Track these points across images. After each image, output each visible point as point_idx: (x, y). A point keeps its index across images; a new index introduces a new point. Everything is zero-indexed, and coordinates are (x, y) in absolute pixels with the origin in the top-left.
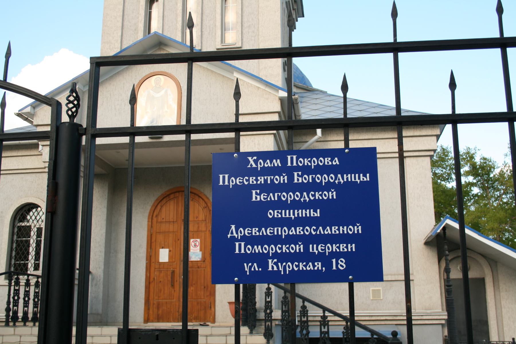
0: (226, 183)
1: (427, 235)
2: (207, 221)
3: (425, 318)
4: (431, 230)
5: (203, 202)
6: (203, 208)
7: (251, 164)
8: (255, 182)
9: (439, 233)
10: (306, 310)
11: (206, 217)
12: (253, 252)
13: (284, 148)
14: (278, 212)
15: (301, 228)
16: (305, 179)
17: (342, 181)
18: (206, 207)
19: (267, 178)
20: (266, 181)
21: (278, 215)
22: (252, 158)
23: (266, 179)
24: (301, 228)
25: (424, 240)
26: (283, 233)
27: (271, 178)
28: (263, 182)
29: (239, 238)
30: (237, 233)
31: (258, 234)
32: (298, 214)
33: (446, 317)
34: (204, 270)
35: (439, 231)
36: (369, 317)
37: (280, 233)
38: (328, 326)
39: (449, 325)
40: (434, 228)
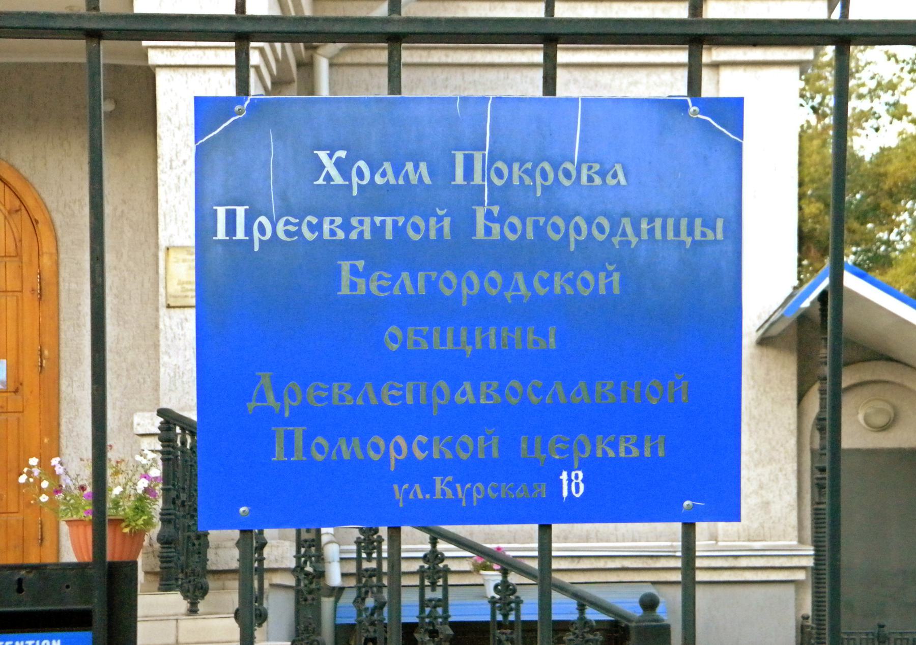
0: (240, 234)
1: (767, 317)
2: (25, 258)
3: (744, 563)
4: (781, 300)
5: (7, 189)
6: (7, 214)
7: (328, 173)
8: (341, 235)
9: (807, 310)
10: (375, 537)
11: (18, 244)
12: (334, 457)
13: (302, 10)
14: (417, 333)
15: (495, 384)
16: (513, 229)
17: (634, 240)
18: (20, 210)
19: (383, 222)
20: (378, 231)
21: (416, 343)
22: (331, 156)
23: (378, 225)
24: (495, 384)
25: (758, 330)
26: (436, 400)
27: (395, 223)
28: (367, 236)
29: (287, 414)
30: (279, 398)
31: (349, 401)
32: (485, 341)
33: (810, 562)
34: (19, 419)
35: (806, 304)
36: (570, 560)
37: (423, 400)
38: (446, 587)
39: (817, 583)
40: (791, 296)
